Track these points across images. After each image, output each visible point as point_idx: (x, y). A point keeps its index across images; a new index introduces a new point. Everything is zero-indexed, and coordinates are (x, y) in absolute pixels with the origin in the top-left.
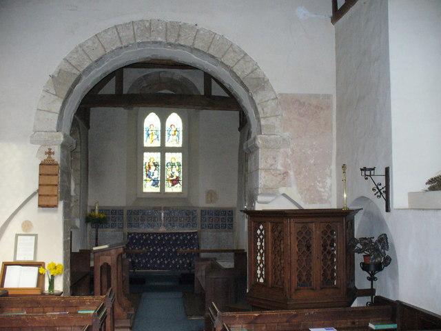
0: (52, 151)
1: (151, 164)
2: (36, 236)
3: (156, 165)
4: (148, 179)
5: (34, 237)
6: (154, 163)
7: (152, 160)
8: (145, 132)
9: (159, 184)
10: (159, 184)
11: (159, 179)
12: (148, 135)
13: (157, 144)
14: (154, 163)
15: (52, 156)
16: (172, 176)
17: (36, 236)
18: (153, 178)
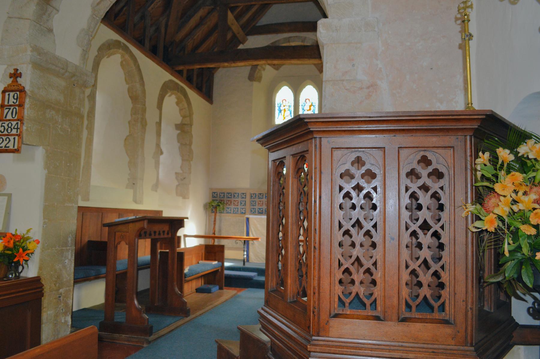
0: (13, 72)
2: (9, 196)
5: (6, 198)
8: (277, 108)
12: (280, 111)
15: (19, 79)
17: (9, 196)
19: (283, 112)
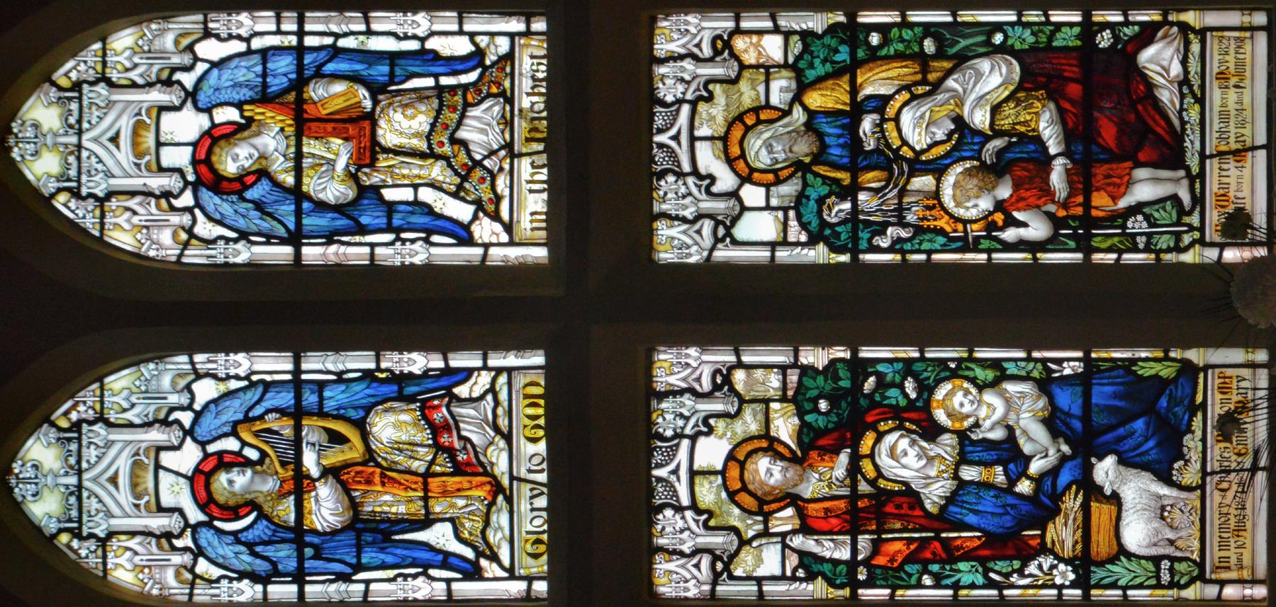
1: (826, 478)
3: (842, 416)
4: (1063, 533)
6: (814, 443)
7: (768, 472)
9: (1147, 359)
10: (1147, 359)
11: (1070, 362)
13: (502, 389)
14: (814, 443)
16: (1019, 162)
18: (1042, 450)
19: (390, 502)
